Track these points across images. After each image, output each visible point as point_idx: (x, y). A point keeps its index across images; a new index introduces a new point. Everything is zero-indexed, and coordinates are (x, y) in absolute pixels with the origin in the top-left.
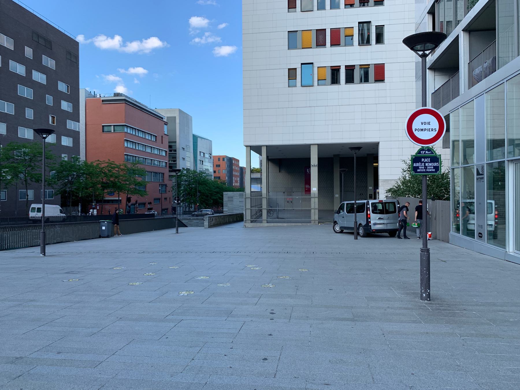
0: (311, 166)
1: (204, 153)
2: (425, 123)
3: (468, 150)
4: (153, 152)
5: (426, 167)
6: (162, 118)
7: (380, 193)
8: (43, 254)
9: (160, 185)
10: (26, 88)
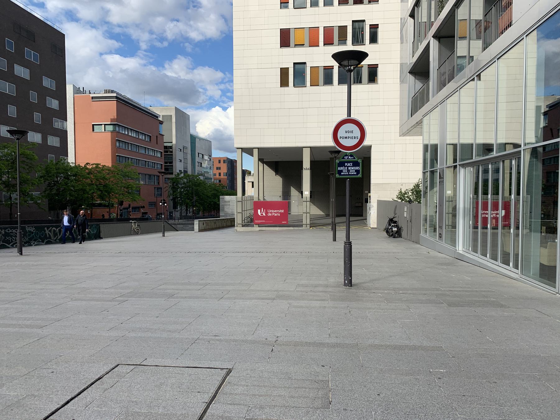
0: (303, 169)
1: (203, 155)
2: (349, 132)
3: (426, 153)
4: (147, 153)
5: (348, 171)
6: (157, 117)
7: (371, 197)
8: (20, 253)
9: (155, 188)
10: (7, 83)
